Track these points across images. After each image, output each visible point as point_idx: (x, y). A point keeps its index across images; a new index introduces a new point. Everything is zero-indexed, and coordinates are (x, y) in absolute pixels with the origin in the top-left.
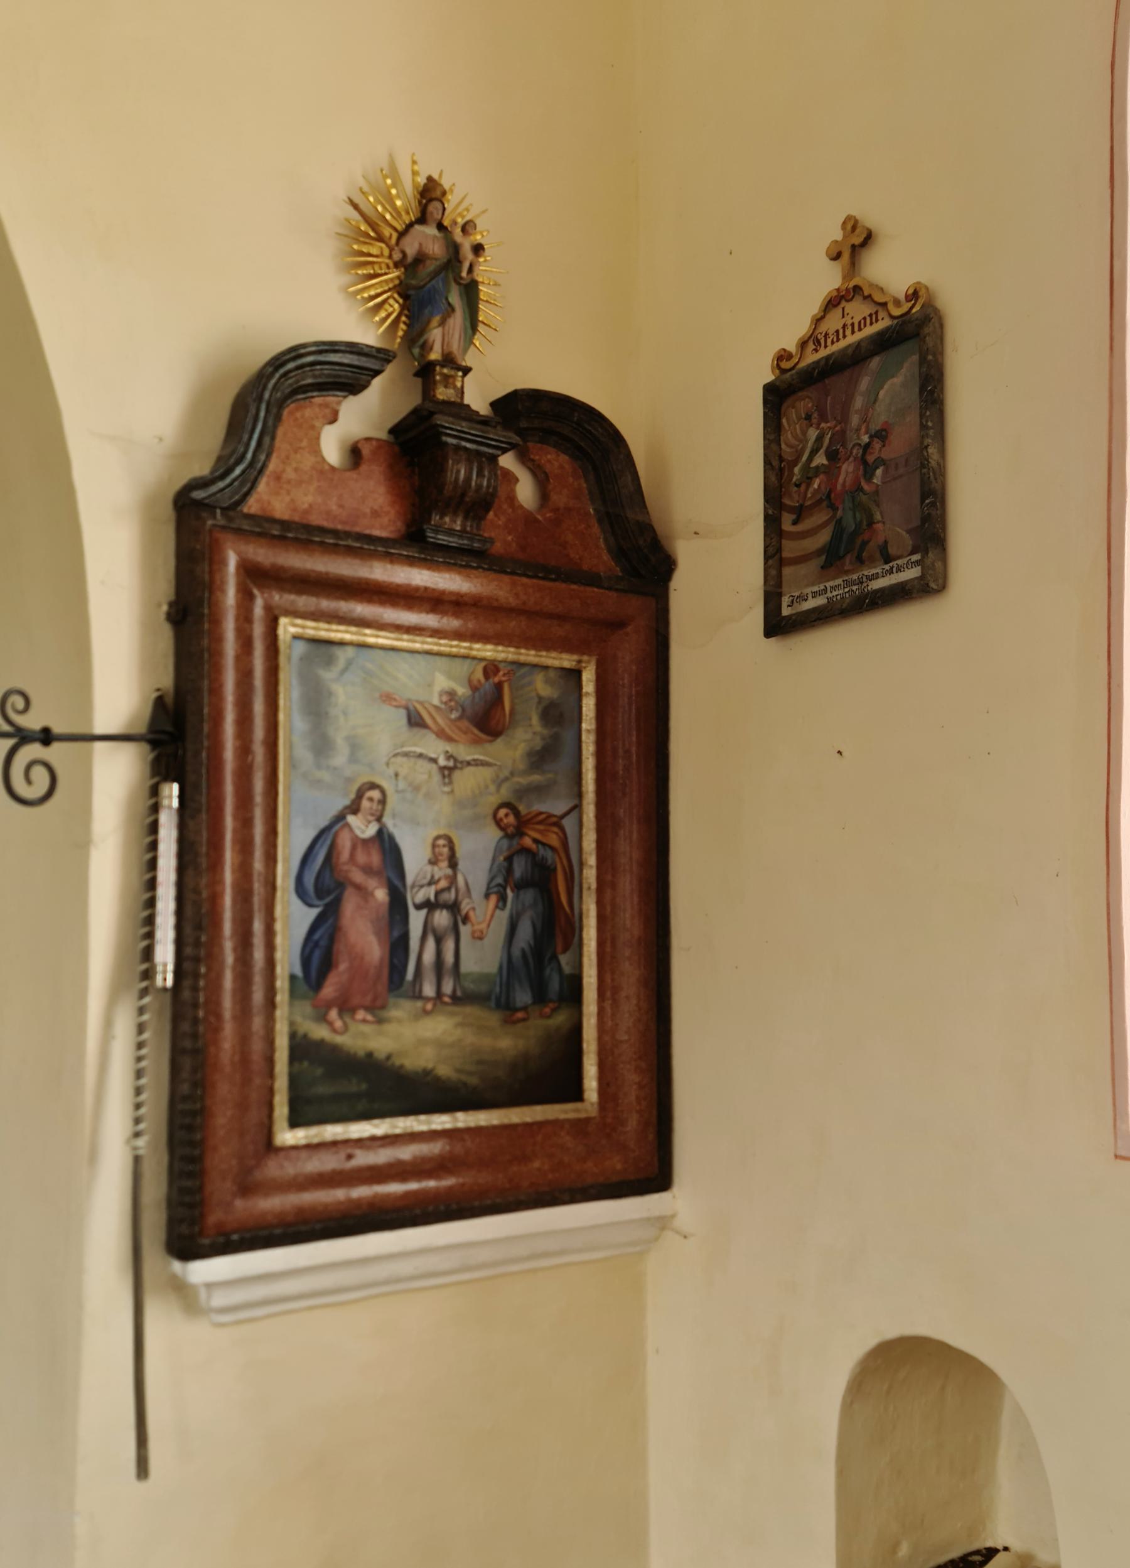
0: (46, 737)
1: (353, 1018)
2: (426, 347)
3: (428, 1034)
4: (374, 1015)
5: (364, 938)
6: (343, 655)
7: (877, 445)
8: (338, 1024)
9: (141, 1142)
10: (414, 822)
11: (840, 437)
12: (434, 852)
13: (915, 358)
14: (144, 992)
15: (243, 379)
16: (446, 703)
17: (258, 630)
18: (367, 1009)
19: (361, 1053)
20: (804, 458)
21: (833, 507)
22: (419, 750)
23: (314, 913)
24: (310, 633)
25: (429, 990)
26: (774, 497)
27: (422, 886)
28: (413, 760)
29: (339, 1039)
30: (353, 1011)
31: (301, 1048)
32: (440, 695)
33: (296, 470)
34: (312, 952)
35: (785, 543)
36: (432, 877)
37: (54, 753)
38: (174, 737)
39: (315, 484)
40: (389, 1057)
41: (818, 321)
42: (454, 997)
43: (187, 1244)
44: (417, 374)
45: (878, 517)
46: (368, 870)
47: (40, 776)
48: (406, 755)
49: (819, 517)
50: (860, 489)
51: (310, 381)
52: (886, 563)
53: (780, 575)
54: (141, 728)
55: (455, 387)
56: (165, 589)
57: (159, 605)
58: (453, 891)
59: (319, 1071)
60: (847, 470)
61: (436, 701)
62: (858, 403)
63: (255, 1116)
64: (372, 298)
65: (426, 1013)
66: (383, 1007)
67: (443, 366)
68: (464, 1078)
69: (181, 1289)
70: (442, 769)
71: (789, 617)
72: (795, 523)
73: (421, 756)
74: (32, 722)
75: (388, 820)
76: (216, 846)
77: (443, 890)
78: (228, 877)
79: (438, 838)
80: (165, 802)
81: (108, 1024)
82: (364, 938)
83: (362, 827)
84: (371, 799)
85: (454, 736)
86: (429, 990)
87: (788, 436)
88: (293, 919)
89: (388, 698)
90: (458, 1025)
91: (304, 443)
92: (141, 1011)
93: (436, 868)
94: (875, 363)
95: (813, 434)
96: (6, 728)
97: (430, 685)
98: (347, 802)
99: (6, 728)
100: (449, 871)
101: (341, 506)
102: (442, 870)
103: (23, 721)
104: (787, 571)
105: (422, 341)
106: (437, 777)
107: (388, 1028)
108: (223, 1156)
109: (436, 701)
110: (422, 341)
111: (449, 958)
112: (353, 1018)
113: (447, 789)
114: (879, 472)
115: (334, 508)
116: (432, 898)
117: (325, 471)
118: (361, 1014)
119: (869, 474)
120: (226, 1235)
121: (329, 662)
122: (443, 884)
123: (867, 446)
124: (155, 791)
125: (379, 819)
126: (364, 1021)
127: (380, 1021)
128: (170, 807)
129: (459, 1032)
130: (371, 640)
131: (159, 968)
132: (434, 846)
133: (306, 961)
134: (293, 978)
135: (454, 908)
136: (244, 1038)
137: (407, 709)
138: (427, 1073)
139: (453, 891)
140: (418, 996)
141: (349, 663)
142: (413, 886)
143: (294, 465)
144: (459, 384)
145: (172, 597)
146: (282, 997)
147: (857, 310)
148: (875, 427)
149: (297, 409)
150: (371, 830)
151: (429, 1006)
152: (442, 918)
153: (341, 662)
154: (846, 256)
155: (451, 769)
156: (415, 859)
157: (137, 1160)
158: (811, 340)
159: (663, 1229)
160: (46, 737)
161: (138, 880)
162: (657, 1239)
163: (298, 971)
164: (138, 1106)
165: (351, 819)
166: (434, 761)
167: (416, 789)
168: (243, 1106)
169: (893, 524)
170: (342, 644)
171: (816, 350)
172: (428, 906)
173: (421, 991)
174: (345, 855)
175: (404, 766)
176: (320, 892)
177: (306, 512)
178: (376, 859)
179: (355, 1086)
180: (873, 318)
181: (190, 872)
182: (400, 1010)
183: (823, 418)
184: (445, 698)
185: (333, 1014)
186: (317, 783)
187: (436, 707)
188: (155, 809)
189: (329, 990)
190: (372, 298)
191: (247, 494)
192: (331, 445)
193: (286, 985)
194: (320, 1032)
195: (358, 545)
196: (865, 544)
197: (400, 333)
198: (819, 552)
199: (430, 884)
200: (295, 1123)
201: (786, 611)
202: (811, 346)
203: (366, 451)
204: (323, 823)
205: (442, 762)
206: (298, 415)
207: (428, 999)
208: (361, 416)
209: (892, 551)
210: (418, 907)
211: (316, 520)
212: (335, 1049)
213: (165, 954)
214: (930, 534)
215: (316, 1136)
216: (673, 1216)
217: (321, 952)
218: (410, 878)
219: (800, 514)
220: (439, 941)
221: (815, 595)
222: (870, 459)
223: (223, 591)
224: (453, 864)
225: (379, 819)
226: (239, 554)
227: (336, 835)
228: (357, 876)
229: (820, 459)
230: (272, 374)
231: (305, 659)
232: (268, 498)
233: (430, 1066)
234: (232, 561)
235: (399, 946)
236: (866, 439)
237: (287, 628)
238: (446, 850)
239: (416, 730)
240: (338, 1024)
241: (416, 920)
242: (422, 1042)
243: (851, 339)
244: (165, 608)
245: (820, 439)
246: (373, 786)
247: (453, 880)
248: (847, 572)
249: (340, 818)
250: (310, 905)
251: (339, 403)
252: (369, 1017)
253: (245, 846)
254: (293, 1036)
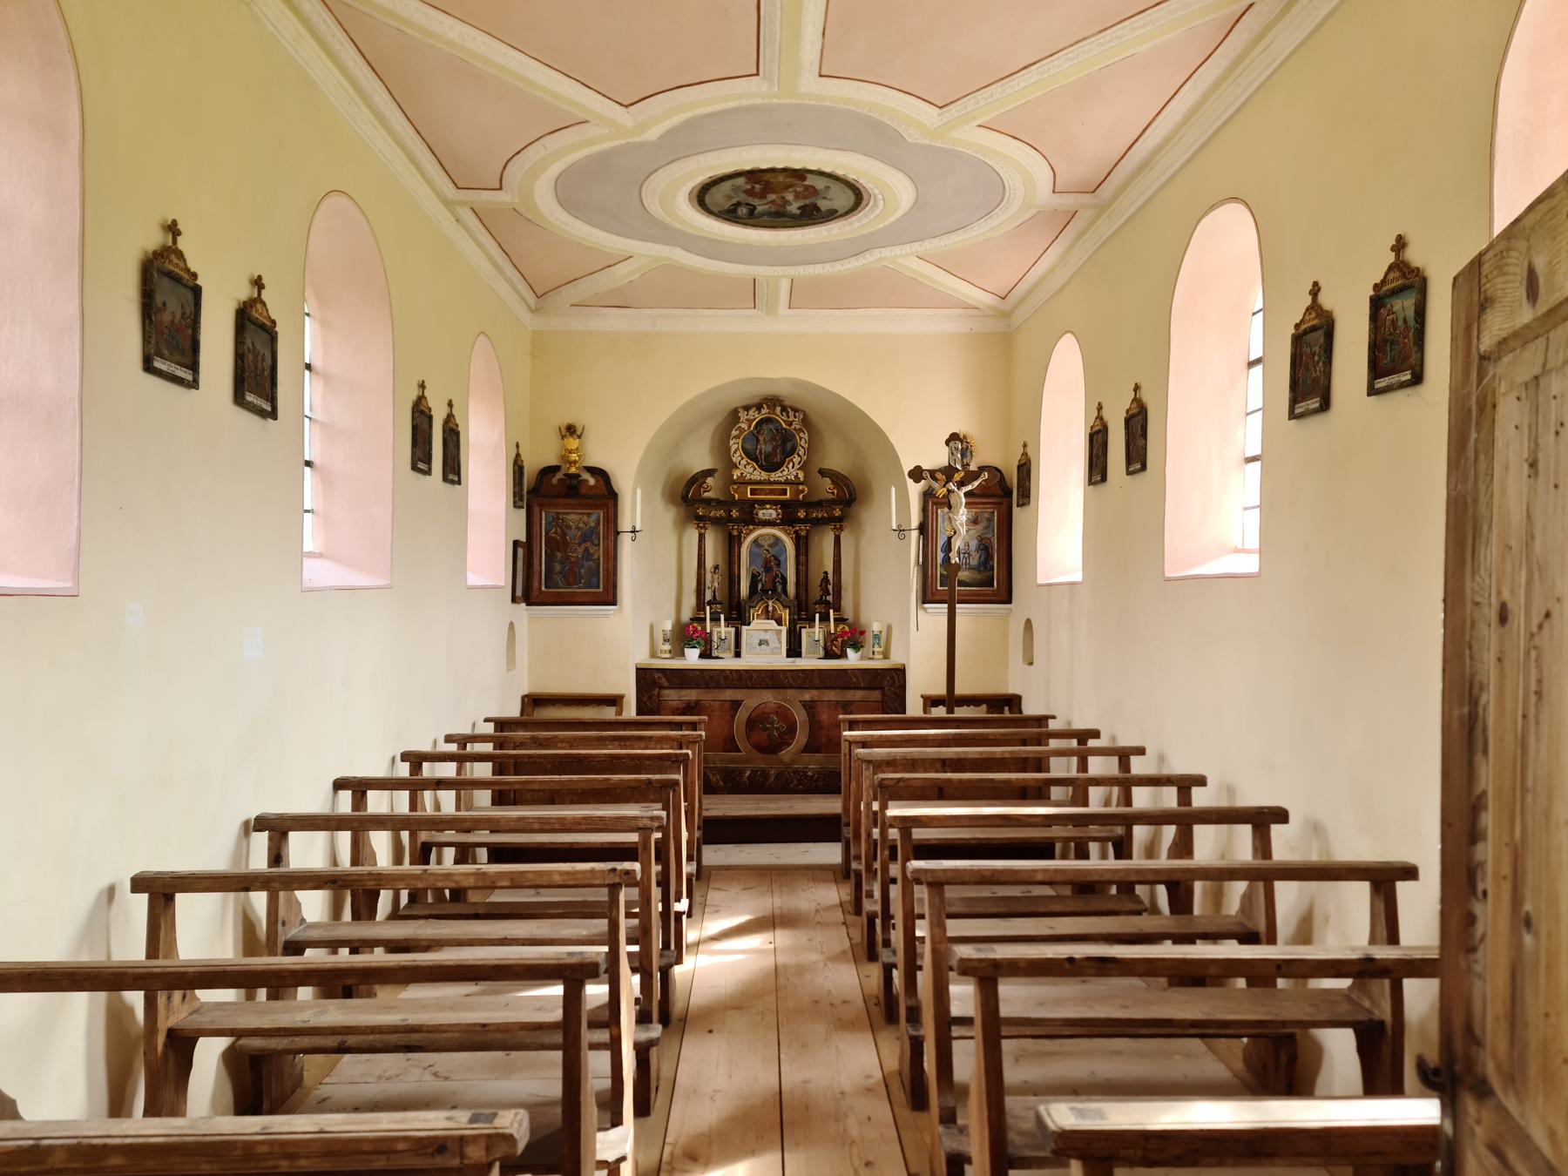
38: (922, 528)
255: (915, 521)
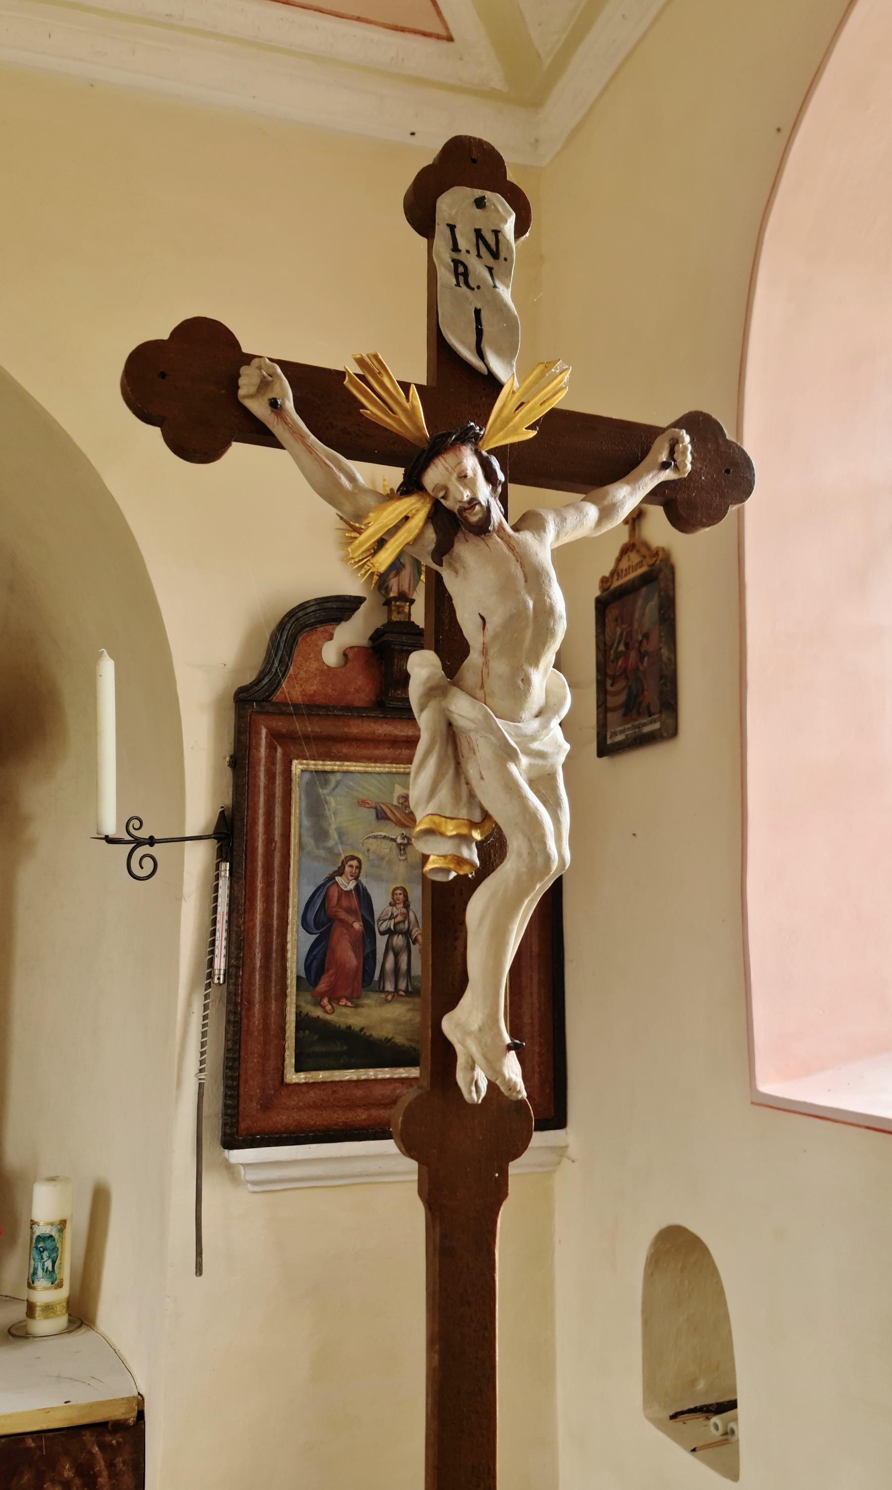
0: (152, 841)
1: (338, 1004)
2: (388, 590)
3: (389, 1015)
4: (352, 1003)
5: (347, 954)
6: (333, 779)
7: (645, 642)
8: (329, 1007)
9: (202, 1075)
10: (378, 879)
11: (630, 634)
12: (393, 899)
13: (657, 594)
14: (208, 986)
15: (274, 625)
16: (402, 804)
17: (279, 768)
18: (347, 999)
19: (343, 1026)
20: (615, 645)
21: (627, 678)
22: (383, 834)
23: (314, 937)
24: (312, 767)
25: (389, 987)
26: (601, 668)
27: (385, 920)
28: (379, 841)
29: (329, 1017)
30: (338, 1000)
31: (302, 1021)
32: (398, 799)
33: (306, 672)
34: (312, 961)
35: (609, 698)
36: (392, 914)
37: (156, 850)
38: (229, 835)
39: (318, 678)
40: (362, 1029)
41: (619, 560)
42: (406, 991)
43: (231, 1142)
44: (384, 604)
45: (646, 687)
46: (349, 911)
47: (148, 864)
48: (375, 837)
49: (621, 684)
50: (638, 668)
51: (313, 621)
52: (650, 716)
53: (605, 718)
54: (210, 832)
55: (403, 612)
56: (228, 748)
57: (225, 758)
58: (407, 922)
59: (316, 1037)
60: (633, 655)
61: (395, 803)
62: (637, 615)
63: (272, 1064)
64: (360, 561)
65: (387, 1001)
66: (358, 997)
67: (396, 601)
68: (413, 1045)
69: (230, 1168)
70: (399, 845)
71: (611, 744)
72: (612, 685)
73: (385, 837)
74: (143, 834)
75: (363, 879)
76: (252, 899)
77: (399, 923)
78: (258, 917)
79: (395, 889)
80: (223, 874)
81: (189, 1004)
82: (347, 954)
83: (347, 884)
84: (351, 866)
85: (407, 824)
86: (389, 987)
87: (608, 630)
88: (298, 943)
89: (363, 803)
90: (409, 1010)
91: (312, 655)
92: (206, 997)
93: (395, 909)
94: (644, 590)
95: (619, 631)
96: (129, 838)
97: (392, 792)
98: (336, 869)
99: (129, 838)
100: (404, 910)
101: (334, 690)
102: (399, 909)
103: (137, 834)
104: (609, 715)
105: (385, 586)
106: (395, 851)
107: (364, 1011)
108: (252, 1087)
109: (395, 803)
110: (385, 586)
111: (404, 966)
112: (338, 1004)
113: (402, 858)
114: (646, 659)
115: (330, 691)
116: (392, 927)
117: (327, 671)
118: (343, 1002)
119: (641, 659)
120: (253, 1135)
121: (326, 783)
122: (399, 918)
123: (641, 642)
124: (217, 868)
125: (356, 878)
126: (346, 1006)
127: (356, 1006)
128: (225, 877)
129: (410, 1015)
130: (352, 768)
131: (217, 972)
132: (393, 894)
133: (308, 968)
134: (299, 978)
135: (407, 934)
136: (265, 1017)
137: (376, 808)
138: (388, 1040)
139: (407, 922)
140: (383, 991)
141: (338, 783)
142: (379, 920)
143: (305, 669)
144: (407, 610)
145: (232, 753)
146: (292, 989)
147: (634, 558)
148: (645, 631)
149: (307, 636)
150: (351, 886)
151: (390, 997)
152: (398, 941)
153: (333, 784)
154: (630, 521)
155: (405, 845)
156: (381, 902)
157: (201, 1086)
158: (615, 572)
159: (562, 1156)
160: (152, 841)
161: (208, 919)
162: (559, 1163)
163: (303, 974)
164: (202, 1054)
165: (338, 879)
166: (394, 840)
167: (382, 858)
168: (264, 1057)
169: (651, 696)
170: (333, 772)
171: (618, 579)
172: (390, 932)
173: (384, 987)
174: (334, 901)
175: (373, 844)
176: (317, 925)
177: (312, 696)
178: (355, 903)
179: (338, 1047)
180: (640, 564)
181: (235, 915)
182: (371, 1000)
183: (623, 623)
184: (401, 801)
185: (325, 1001)
186: (317, 858)
187: (395, 806)
188: (217, 877)
189: (322, 986)
190: (360, 561)
191: (276, 689)
192: (330, 654)
193: (294, 982)
194: (317, 1012)
195: (341, 713)
196: (641, 703)
197: (374, 582)
198: (622, 706)
199: (390, 919)
200: (298, 1070)
201: (609, 742)
202: (616, 577)
203: (350, 655)
204: (320, 881)
205: (399, 841)
206: (308, 639)
207: (389, 993)
208: (350, 634)
209: (652, 709)
210: (382, 934)
211: (319, 699)
212: (326, 1023)
213: (220, 963)
214: (669, 704)
215: (312, 1078)
216: (567, 1147)
217: (317, 964)
218: (377, 916)
219: (615, 679)
220: (397, 955)
221: (622, 732)
222: (643, 650)
223: (258, 750)
224: (407, 905)
225: (356, 878)
226: (266, 727)
227: (328, 889)
228: (343, 915)
229: (622, 648)
230: (288, 621)
231: (311, 785)
232: (291, 690)
233: (390, 1036)
234: (264, 731)
235: (369, 958)
236: (640, 637)
237: (297, 766)
238: (402, 896)
239: (382, 821)
240: (329, 1007)
241: (381, 942)
242: (387, 1021)
243: (632, 575)
244: (228, 759)
245: (621, 634)
246: (353, 858)
247: (406, 916)
248: (634, 720)
249: (331, 878)
250: (311, 934)
251: (334, 629)
252: (349, 1004)
253: (268, 899)
254: (298, 1014)
255: (200, 799)
